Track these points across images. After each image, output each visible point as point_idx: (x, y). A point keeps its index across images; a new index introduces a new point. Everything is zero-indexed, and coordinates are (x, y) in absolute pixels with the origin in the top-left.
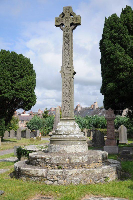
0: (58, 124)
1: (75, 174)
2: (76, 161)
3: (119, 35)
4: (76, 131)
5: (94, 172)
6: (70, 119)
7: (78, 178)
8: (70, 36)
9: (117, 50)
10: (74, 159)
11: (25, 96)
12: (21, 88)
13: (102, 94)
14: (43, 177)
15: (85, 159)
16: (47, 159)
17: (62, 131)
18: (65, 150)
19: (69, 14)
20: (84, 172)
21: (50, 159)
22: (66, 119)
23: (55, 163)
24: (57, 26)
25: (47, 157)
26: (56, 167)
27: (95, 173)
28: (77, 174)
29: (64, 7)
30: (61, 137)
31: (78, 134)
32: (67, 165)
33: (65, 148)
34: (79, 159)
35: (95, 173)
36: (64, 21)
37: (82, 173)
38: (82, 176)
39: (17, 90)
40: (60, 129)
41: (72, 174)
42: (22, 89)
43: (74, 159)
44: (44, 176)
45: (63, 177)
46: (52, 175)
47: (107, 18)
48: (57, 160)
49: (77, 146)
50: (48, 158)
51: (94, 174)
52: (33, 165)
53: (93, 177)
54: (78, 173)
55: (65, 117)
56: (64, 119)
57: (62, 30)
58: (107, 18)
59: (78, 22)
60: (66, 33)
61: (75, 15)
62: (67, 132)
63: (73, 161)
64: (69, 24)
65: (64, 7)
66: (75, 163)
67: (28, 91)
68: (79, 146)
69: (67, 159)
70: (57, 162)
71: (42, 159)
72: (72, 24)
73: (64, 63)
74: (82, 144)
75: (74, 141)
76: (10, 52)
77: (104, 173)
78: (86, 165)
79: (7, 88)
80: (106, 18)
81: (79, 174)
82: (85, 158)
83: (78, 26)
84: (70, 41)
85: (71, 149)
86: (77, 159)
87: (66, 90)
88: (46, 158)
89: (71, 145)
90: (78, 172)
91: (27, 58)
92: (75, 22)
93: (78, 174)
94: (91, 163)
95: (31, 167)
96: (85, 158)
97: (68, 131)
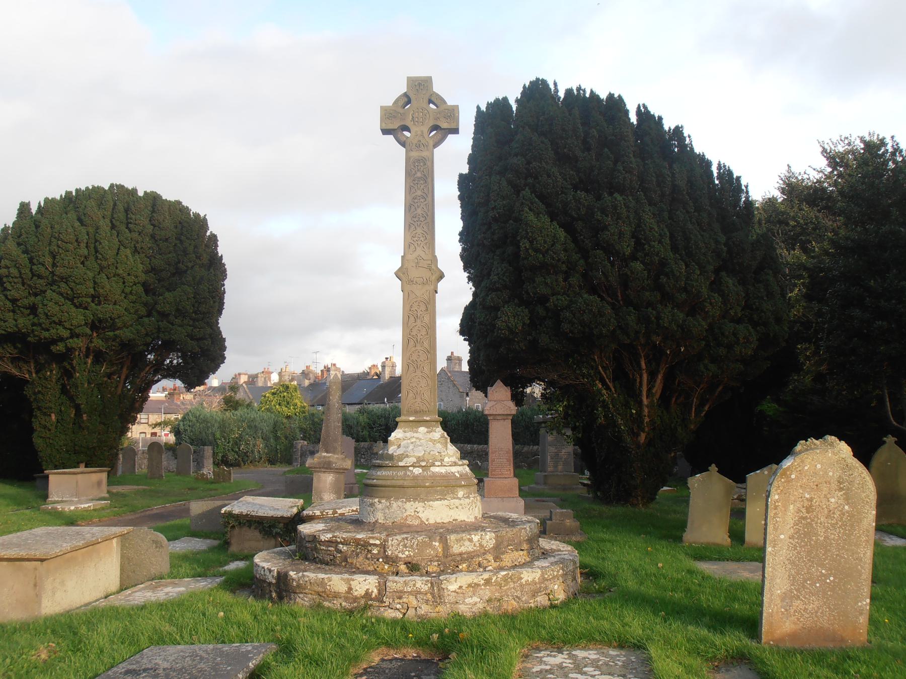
0: (393, 434)
1: (470, 586)
2: (463, 549)
3: (529, 163)
5: (522, 578)
6: (428, 419)
8: (429, 163)
9: (526, 209)
11: (192, 337)
12: (178, 310)
15: (489, 539)
16: (375, 545)
17: (407, 456)
19: (426, 101)
20: (494, 579)
23: (400, 555)
24: (385, 132)
25: (373, 538)
26: (403, 567)
27: (523, 581)
28: (474, 586)
29: (408, 78)
30: (405, 474)
31: (455, 464)
32: (437, 561)
33: (420, 509)
34: (471, 540)
35: (523, 581)
38: (487, 593)
39: (163, 315)
41: (460, 587)
44: (374, 596)
45: (433, 597)
46: (400, 595)
48: (405, 546)
49: (457, 502)
50: (378, 542)
51: (521, 585)
52: (322, 562)
53: (519, 594)
54: (475, 584)
55: (416, 412)
56: (411, 419)
57: (403, 144)
59: (453, 126)
60: (415, 154)
61: (445, 102)
62: (423, 461)
63: (456, 549)
64: (425, 129)
65: (408, 78)
66: (461, 554)
68: (462, 502)
69: (437, 544)
70: (407, 553)
71: (357, 542)
72: (436, 128)
74: (468, 497)
75: (445, 487)
77: (545, 580)
78: (491, 558)
81: (478, 585)
82: (488, 537)
83: (451, 137)
84: (429, 180)
86: (467, 543)
87: (416, 328)
88: (372, 541)
90: (475, 581)
92: (444, 125)
94: (503, 553)
95: (326, 572)
96: (488, 537)
97: (426, 457)
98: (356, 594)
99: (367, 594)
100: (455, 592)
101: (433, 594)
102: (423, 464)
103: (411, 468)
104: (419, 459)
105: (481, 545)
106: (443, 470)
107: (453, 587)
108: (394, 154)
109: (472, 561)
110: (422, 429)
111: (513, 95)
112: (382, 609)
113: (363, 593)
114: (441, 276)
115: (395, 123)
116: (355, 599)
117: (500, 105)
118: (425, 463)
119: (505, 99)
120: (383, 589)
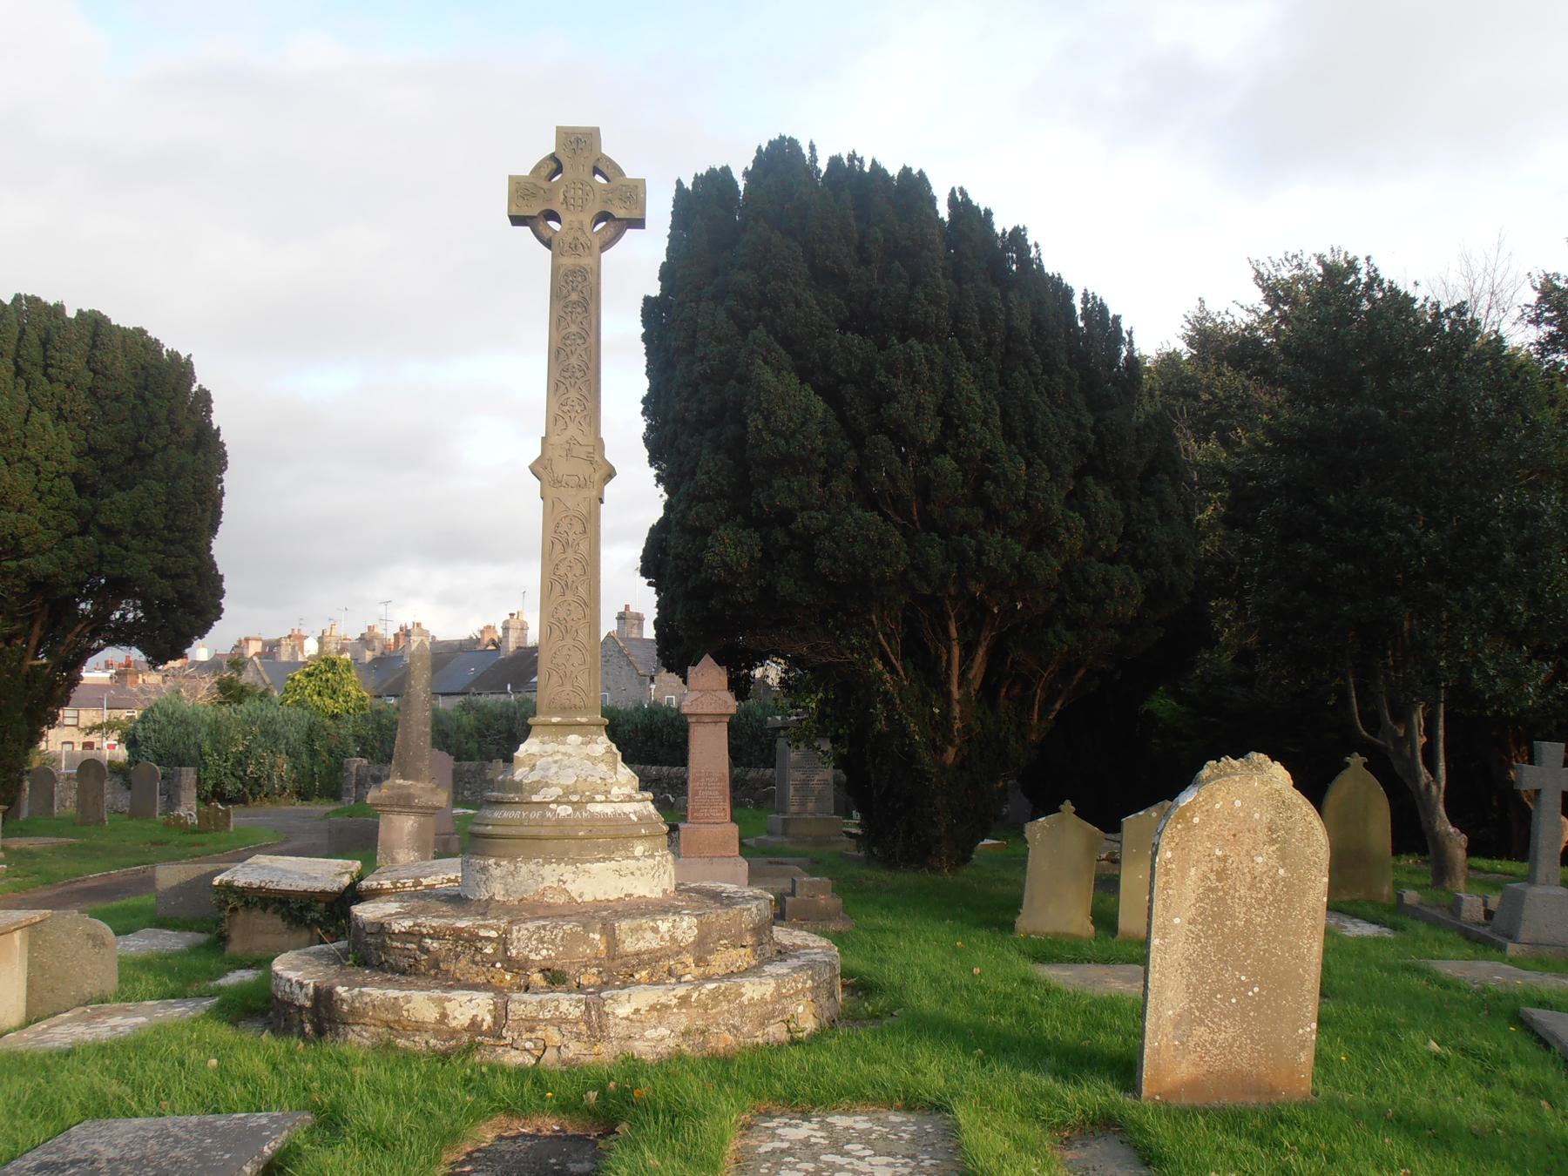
0: (522, 747)
1: (652, 1008)
2: (642, 945)
4: (620, 786)
5: (742, 995)
6: (584, 720)
7: (663, 1031)
8: (592, 279)
10: (633, 931)
12: (137, 524)
13: (650, 584)
14: (481, 1034)
16: (488, 939)
17: (547, 785)
18: (569, 887)
20: (695, 995)
21: (503, 942)
22: (565, 721)
23: (533, 956)
24: (517, 220)
25: (485, 927)
26: (537, 978)
28: (659, 1009)
31: (630, 799)
34: (655, 930)
36: (562, 197)
37: (684, 1001)
38: (682, 1020)
39: (110, 532)
40: (534, 777)
41: (637, 1011)
42: (141, 529)
43: (633, 931)
44: (485, 1027)
46: (531, 1025)
47: (688, 184)
48: (541, 940)
49: (632, 864)
50: (493, 934)
51: (741, 1006)
52: (394, 969)
53: (737, 1021)
55: (563, 709)
56: (555, 720)
58: (688, 184)
59: (635, 215)
60: (568, 261)
61: (622, 174)
62: (575, 793)
63: (630, 945)
64: (587, 219)
66: (638, 954)
67: (172, 542)
69: (597, 937)
70: (544, 952)
71: (457, 934)
72: (604, 216)
73: (555, 419)
74: (652, 856)
75: (612, 838)
76: (71, 313)
78: (690, 960)
79: (52, 524)
80: (679, 183)
82: (685, 925)
84: (592, 307)
85: (595, 882)
86: (649, 935)
87: (567, 563)
88: (483, 933)
89: (598, 861)
91: (174, 356)
92: (620, 213)
93: (666, 1007)
96: (685, 925)
98: (454, 1024)
99: (474, 1025)
100: (627, 1018)
101: (588, 1023)
102: (575, 798)
103: (553, 806)
104: (568, 791)
105: (673, 939)
106: (608, 809)
107: (624, 1011)
108: (531, 261)
109: (658, 967)
110: (574, 739)
111: (740, 164)
112: (500, 1050)
113: (467, 1023)
114: (611, 474)
115: (533, 208)
116: (454, 1033)
117: (717, 180)
118: (578, 796)
119: (726, 171)
120: (501, 1014)
